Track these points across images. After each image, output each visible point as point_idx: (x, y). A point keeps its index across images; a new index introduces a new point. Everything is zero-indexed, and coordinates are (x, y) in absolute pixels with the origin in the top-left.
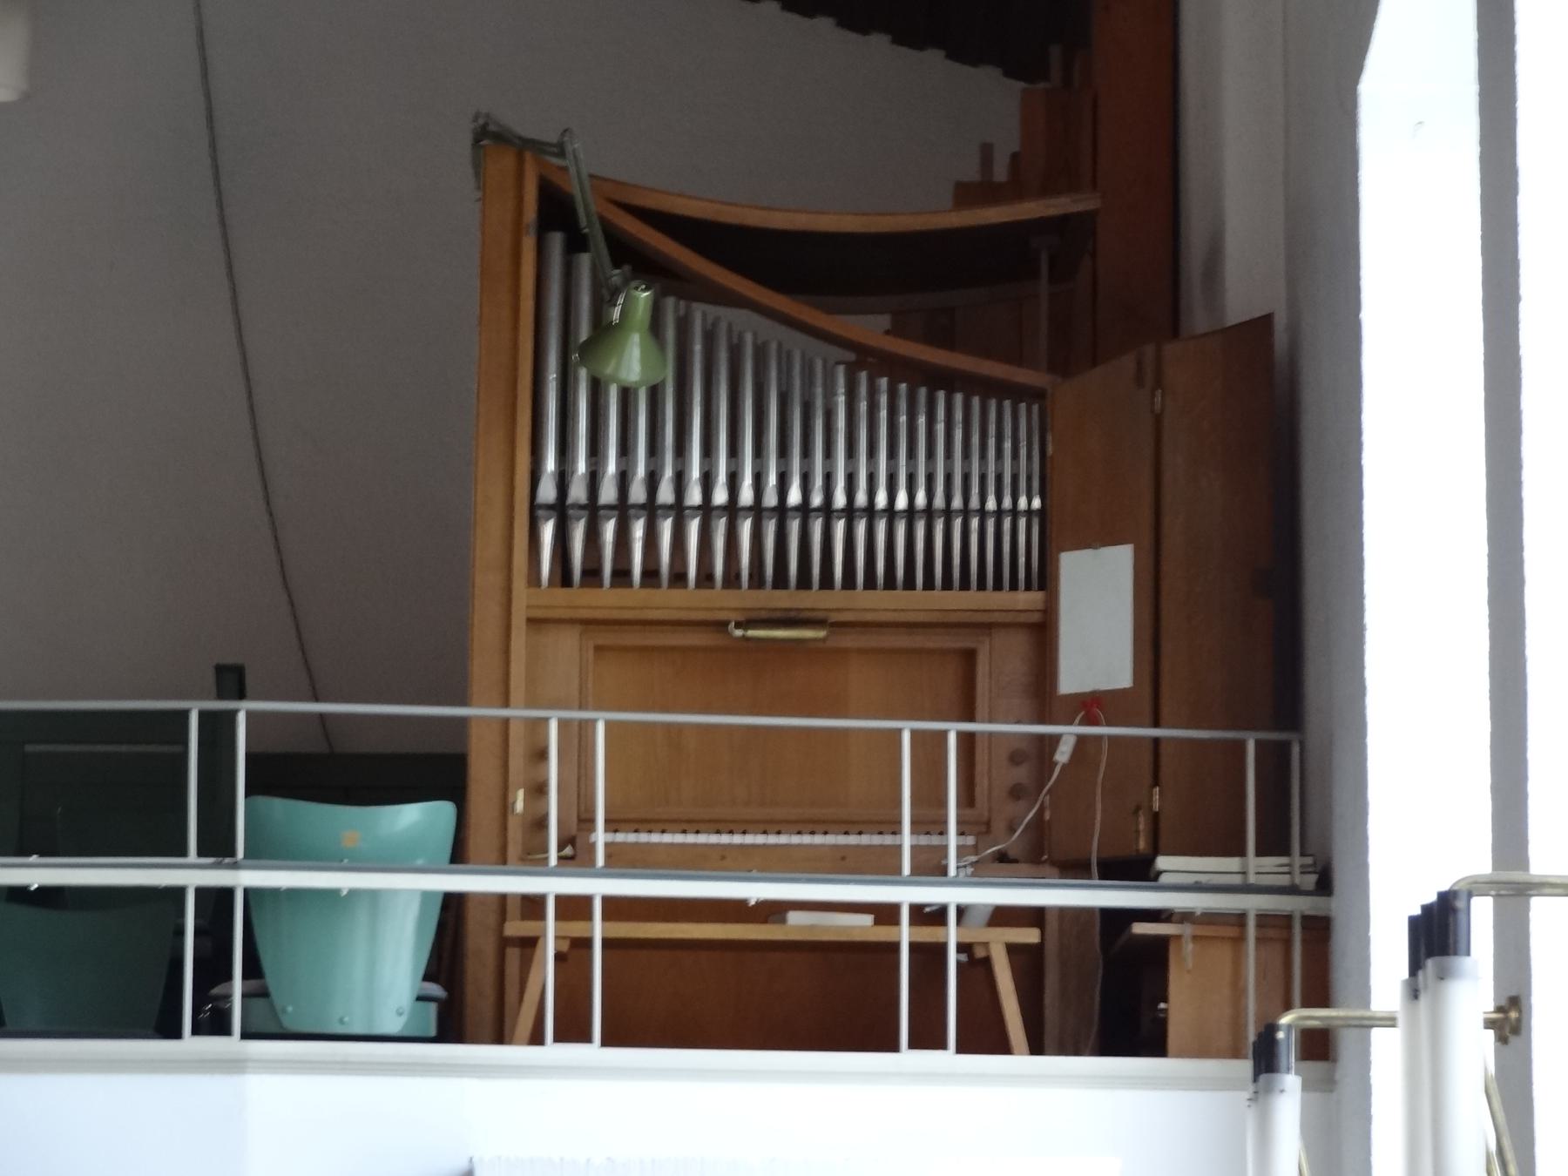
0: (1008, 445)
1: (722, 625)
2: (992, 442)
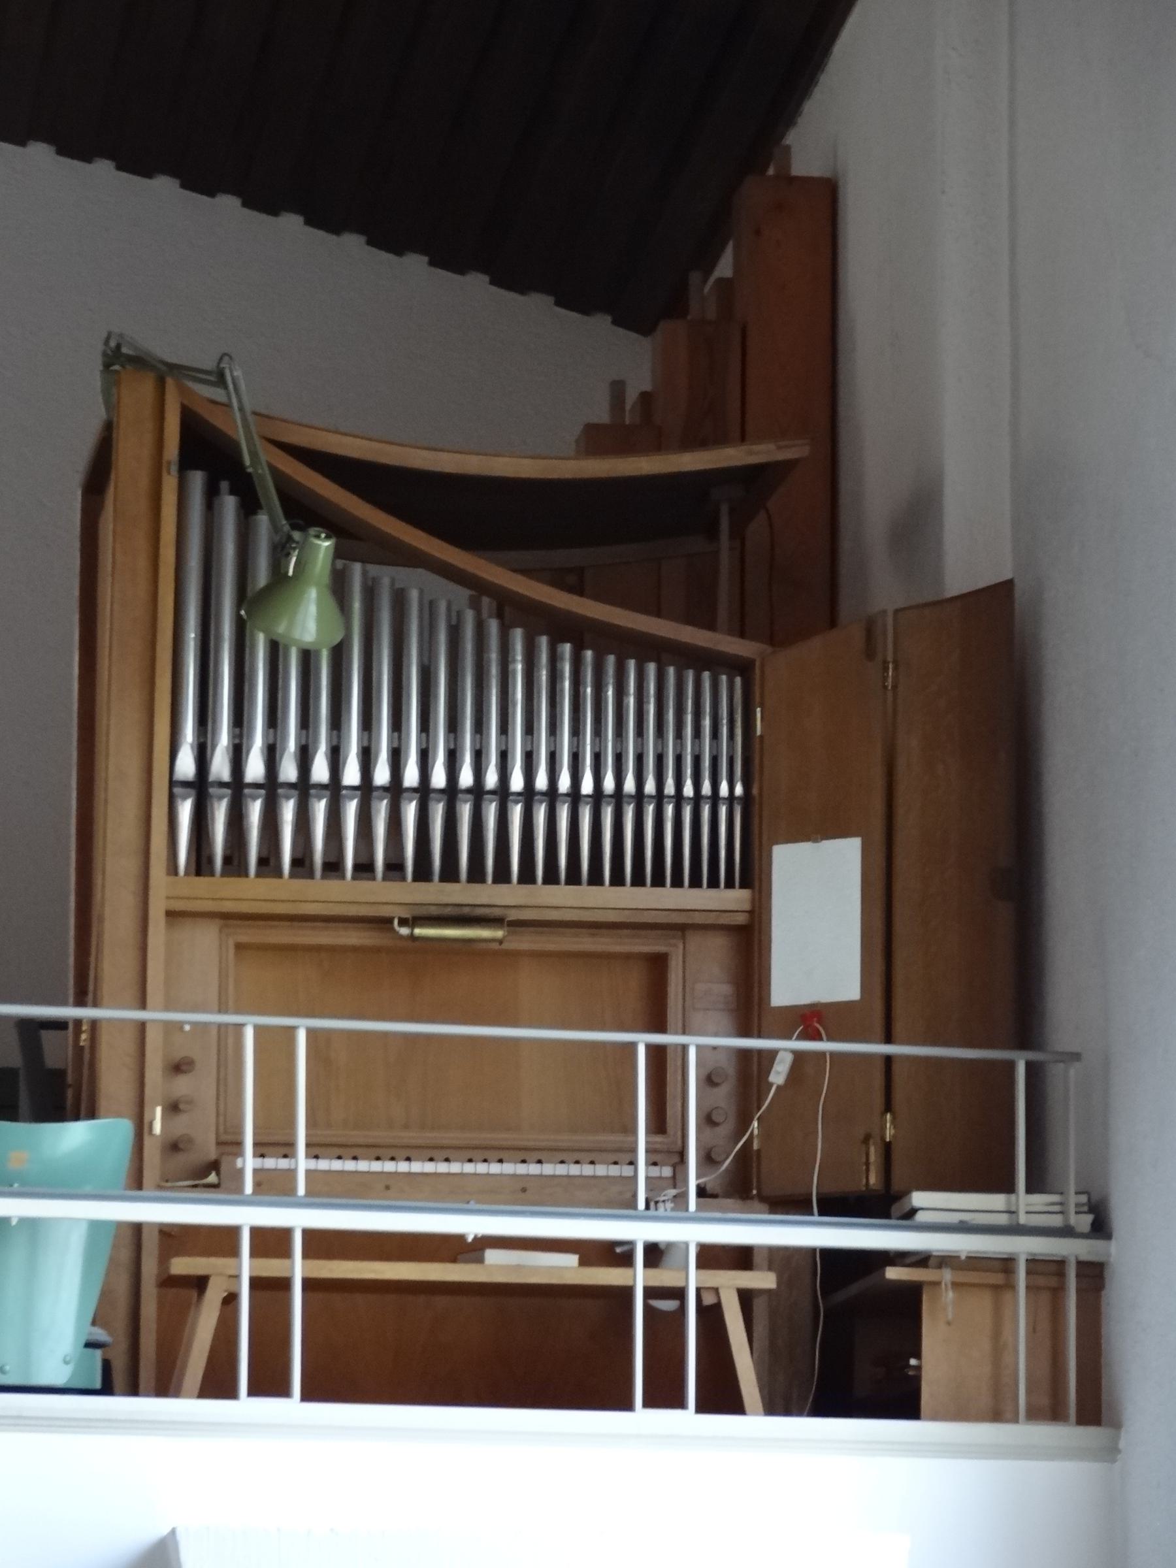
0: (707, 722)
1: (384, 923)
2: (689, 718)
